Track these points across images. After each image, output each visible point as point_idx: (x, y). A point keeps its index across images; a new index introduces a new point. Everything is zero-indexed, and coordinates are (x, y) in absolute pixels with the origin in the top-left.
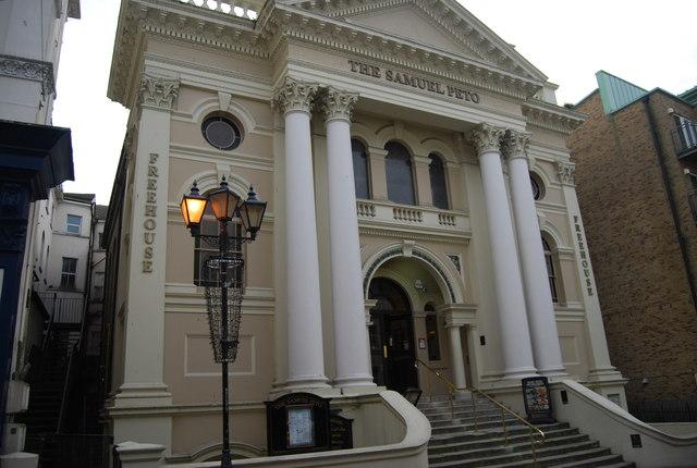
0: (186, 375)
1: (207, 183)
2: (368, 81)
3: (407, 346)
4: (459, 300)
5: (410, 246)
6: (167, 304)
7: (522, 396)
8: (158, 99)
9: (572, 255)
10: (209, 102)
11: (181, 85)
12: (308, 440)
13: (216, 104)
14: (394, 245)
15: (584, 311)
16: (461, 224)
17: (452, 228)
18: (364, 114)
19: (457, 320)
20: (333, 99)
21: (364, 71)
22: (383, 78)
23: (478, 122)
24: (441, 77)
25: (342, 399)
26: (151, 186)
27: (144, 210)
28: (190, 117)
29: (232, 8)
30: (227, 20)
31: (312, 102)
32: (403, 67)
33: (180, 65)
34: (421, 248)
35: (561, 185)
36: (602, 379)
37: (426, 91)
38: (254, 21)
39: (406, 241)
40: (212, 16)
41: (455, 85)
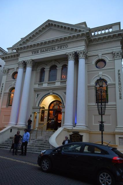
6: (1, 110)
7: (101, 136)
8: (118, 57)
10: (96, 58)
11: (9, 69)
13: (98, 58)
15: (116, 105)
18: (36, 64)
24: (38, 49)
25: (72, 130)
27: (118, 84)
29: (98, 32)
31: (33, 63)
32: (44, 48)
35: (114, 60)
40: (104, 35)
41: (33, 51)
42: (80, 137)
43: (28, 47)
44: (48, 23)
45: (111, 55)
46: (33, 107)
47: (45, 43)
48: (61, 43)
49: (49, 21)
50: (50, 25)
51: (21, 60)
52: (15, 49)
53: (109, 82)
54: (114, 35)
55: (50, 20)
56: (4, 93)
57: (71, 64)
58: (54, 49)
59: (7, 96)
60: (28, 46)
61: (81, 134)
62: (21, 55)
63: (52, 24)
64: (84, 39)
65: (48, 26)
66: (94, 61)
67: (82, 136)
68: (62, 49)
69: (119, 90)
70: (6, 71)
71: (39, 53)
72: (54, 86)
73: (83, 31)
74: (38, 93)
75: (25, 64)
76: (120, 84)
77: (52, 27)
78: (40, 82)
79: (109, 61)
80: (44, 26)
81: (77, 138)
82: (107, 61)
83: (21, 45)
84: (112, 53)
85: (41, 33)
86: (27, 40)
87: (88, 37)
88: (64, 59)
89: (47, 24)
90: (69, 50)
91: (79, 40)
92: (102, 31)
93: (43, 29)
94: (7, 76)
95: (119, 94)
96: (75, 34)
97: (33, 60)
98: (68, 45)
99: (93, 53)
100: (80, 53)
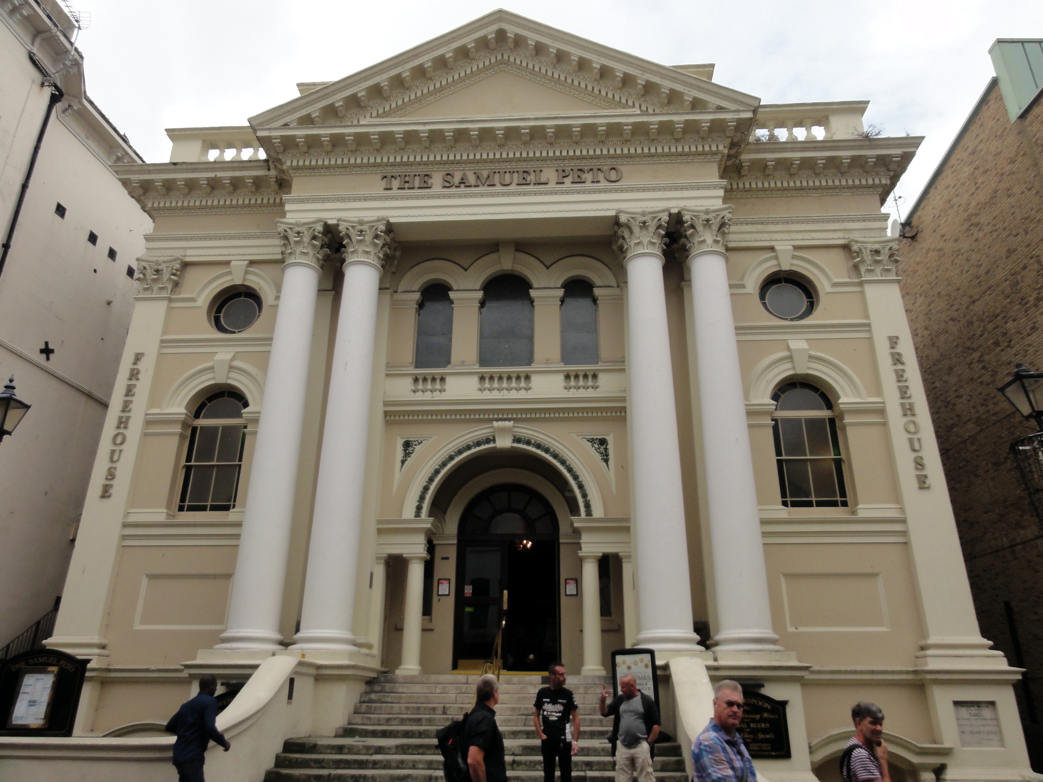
0: (138, 627)
1: (204, 378)
2: (417, 198)
3: (468, 590)
4: (598, 511)
5: (503, 430)
6: (124, 537)
8: (878, 269)
9: (882, 412)
11: (186, 265)
12: (520, 752)
14: (481, 432)
15: (903, 521)
16: (607, 385)
17: (590, 393)
18: (402, 251)
19: (593, 546)
20: (692, 226)
21: (406, 184)
22: (437, 188)
23: (613, 213)
26: (129, 392)
28: (193, 300)
29: (808, 130)
30: (234, 169)
33: (838, 221)
34: (526, 431)
35: (861, 284)
36: (933, 665)
37: (513, 187)
38: (266, 161)
39: (495, 424)
41: (390, 171)
42: (772, 711)
43: (309, 147)
44: (495, 27)
45: (838, 257)
46: (379, 522)
47: (486, 135)
48: (582, 153)
49: (500, 20)
50: (500, 44)
51: (306, 209)
52: (264, 142)
53: (846, 398)
54: (804, 161)
55: (506, 13)
56: (149, 423)
57: (645, 272)
58: (531, 178)
59: (176, 439)
60: (361, 140)
61: (774, 692)
62: (300, 187)
63: (519, 41)
64: (715, 153)
65: (493, 46)
66: (758, 271)
67: (784, 704)
68: (588, 185)
69: (907, 446)
70: (166, 276)
71: (437, 188)
72: (522, 395)
73: (720, 109)
74: (412, 433)
75: (333, 249)
76: (908, 411)
77: (518, 58)
78: (417, 366)
79: (836, 285)
80: (469, 41)
81: (753, 721)
82: (823, 286)
83: (307, 120)
84: (846, 247)
85: (445, 79)
86: (354, 102)
87: (733, 145)
88: (605, 243)
89: (490, 31)
90: (639, 198)
91: (687, 155)
92: (227, 151)
93: (463, 53)
94: (170, 309)
95: (912, 465)
96: (675, 118)
97: (390, 228)
98: (625, 169)
99: (747, 237)
100: (352, 232)
